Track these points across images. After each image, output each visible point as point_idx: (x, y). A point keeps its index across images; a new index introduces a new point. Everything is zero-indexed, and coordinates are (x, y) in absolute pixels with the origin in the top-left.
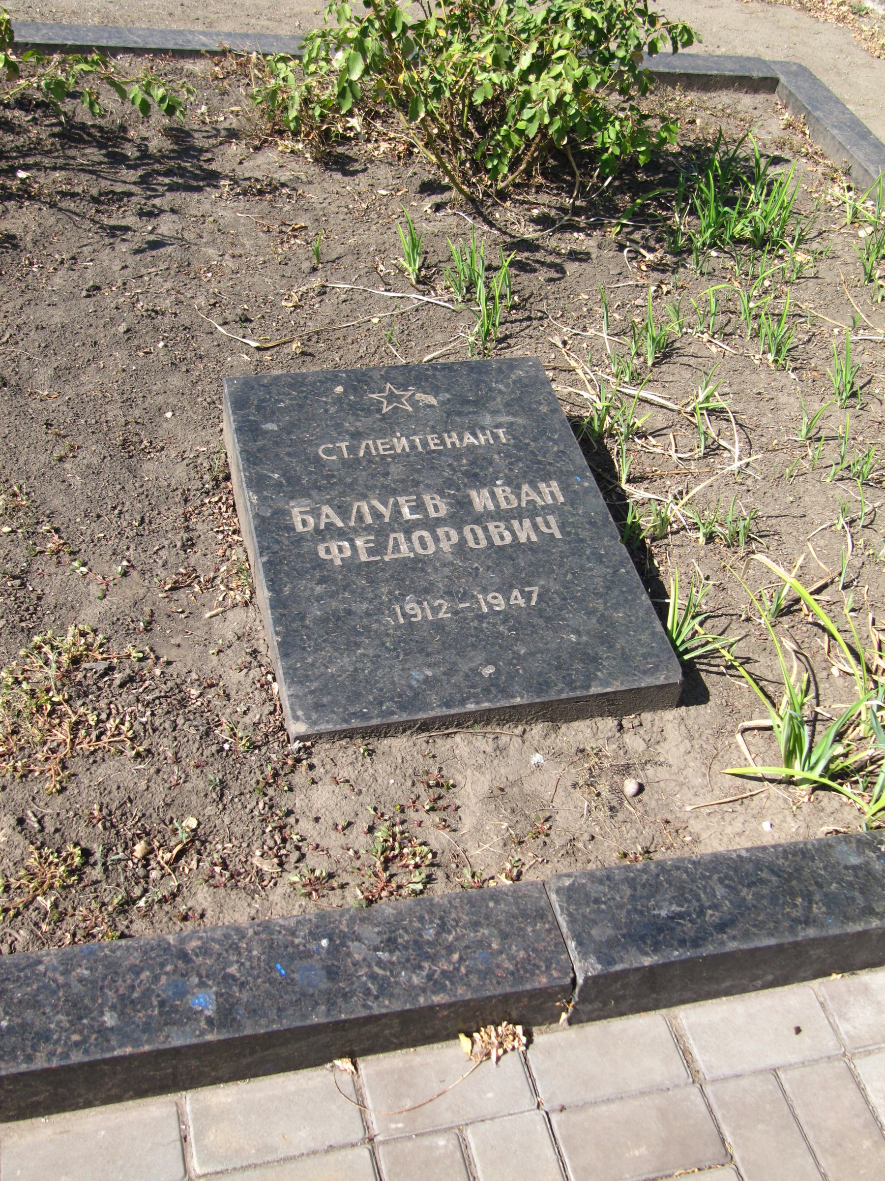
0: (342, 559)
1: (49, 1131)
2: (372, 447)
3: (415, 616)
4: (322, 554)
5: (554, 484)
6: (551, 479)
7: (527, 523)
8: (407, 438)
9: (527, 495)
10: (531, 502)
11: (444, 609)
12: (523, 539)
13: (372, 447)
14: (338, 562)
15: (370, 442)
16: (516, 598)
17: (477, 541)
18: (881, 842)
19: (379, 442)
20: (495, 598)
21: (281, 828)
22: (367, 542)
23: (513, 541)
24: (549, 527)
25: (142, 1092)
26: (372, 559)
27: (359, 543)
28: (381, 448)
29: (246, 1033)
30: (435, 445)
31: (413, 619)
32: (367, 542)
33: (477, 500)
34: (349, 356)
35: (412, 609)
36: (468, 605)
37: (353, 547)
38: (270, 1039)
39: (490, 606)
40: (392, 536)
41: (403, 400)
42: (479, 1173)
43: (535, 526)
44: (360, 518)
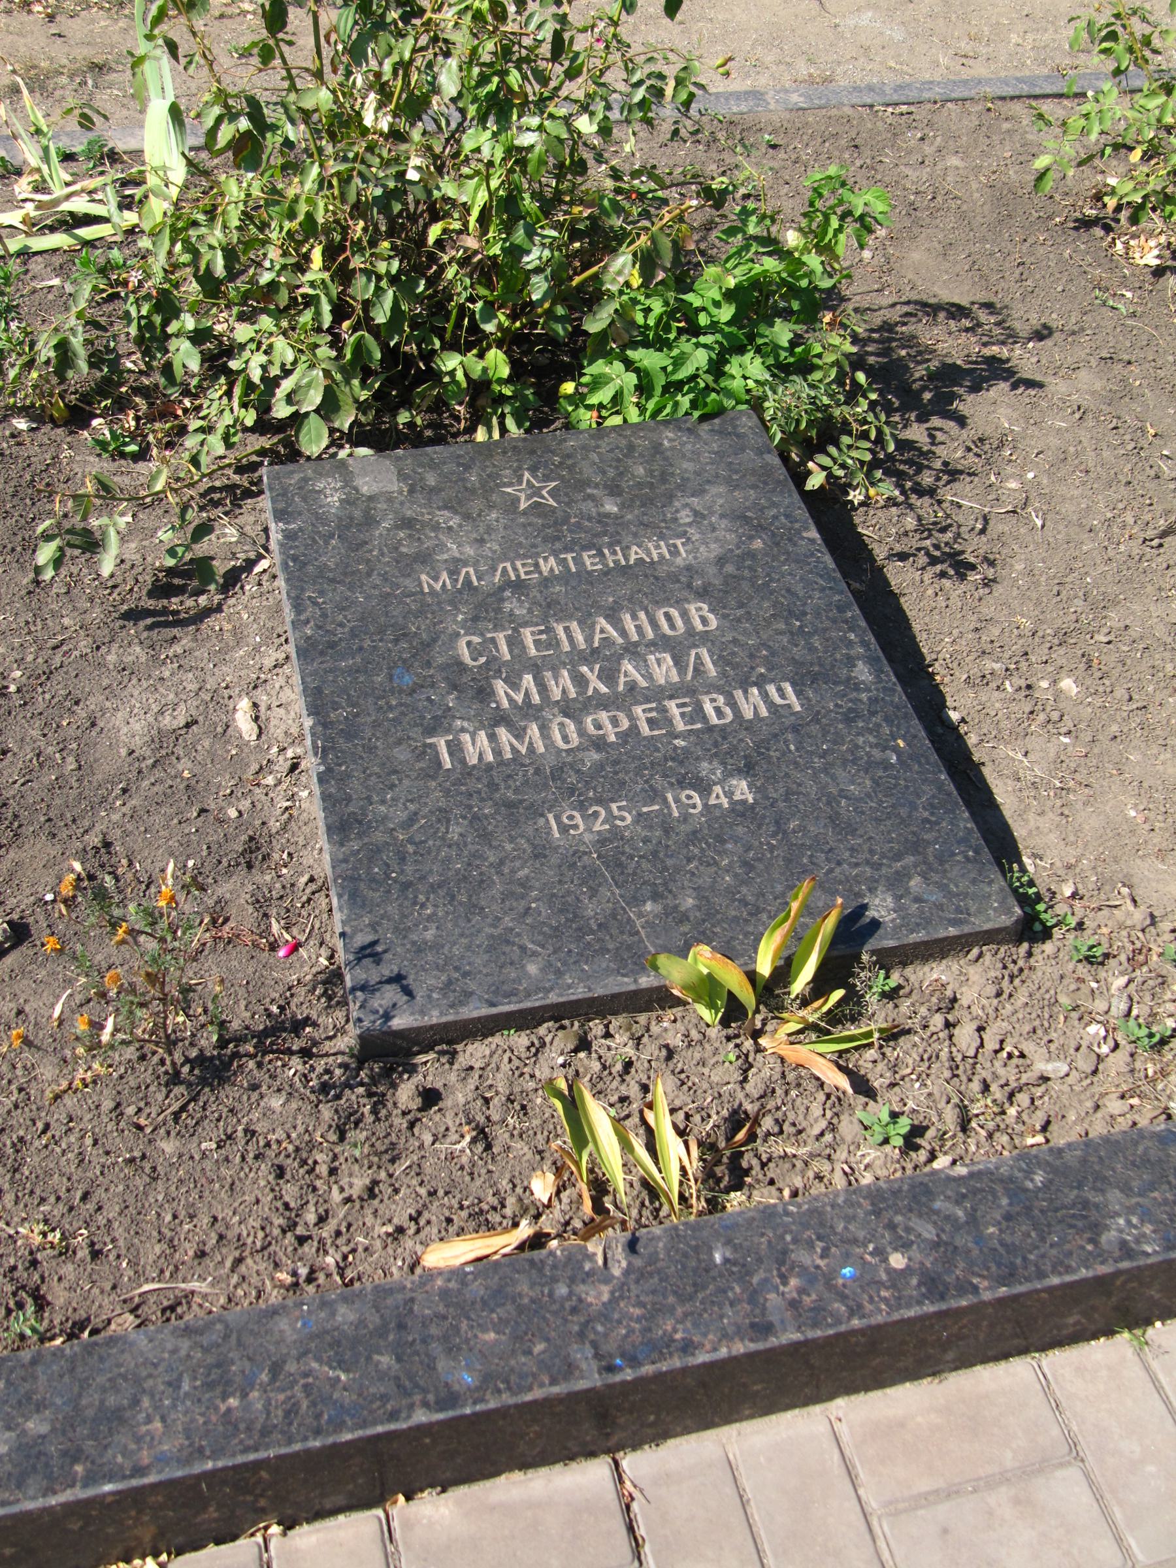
0: (616, 734)
1: (313, 1539)
2: (510, 569)
7: (556, 695)
8: (556, 557)
13: (510, 569)
15: (508, 565)
16: (718, 797)
19: (518, 564)
22: (684, 705)
25: (769, 1406)
26: (656, 733)
27: (638, 710)
28: (522, 571)
29: (582, 1385)
31: (618, 823)
32: (684, 705)
36: (656, 807)
37: (632, 718)
38: (875, 1336)
41: (544, 492)
42: (769, 1560)
43: (765, 696)
44: (699, 670)
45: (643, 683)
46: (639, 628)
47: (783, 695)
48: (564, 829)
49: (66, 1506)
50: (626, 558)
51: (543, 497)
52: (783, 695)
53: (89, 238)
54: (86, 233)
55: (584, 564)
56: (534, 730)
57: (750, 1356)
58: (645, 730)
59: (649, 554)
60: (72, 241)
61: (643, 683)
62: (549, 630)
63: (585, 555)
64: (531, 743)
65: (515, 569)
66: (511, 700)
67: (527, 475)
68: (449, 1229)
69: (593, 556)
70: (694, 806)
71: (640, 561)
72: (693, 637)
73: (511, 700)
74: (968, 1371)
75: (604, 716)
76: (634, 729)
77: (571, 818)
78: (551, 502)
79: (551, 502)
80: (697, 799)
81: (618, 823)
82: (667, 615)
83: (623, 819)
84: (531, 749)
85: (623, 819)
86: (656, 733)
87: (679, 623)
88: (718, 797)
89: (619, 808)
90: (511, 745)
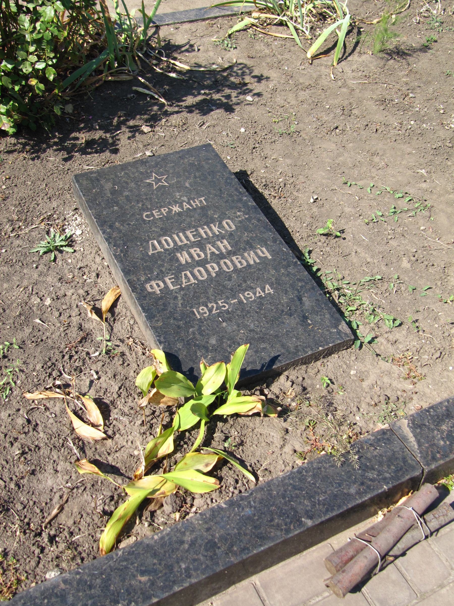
3: (251, 298)
4: (150, 290)
5: (225, 242)
6: (183, 250)
9: (210, 249)
10: (213, 254)
11: (215, 309)
12: (252, 262)
14: (159, 292)
16: (259, 293)
17: (228, 267)
18: (136, 603)
20: (248, 294)
21: (43, 518)
23: (234, 268)
24: (264, 253)
31: (223, 309)
33: (181, 258)
34: (43, 195)
35: (202, 309)
39: (247, 299)
40: (183, 273)
43: (256, 254)
45: (217, 252)
46: (205, 232)
47: (264, 253)
48: (247, 299)
51: (163, 183)
57: (169, 596)
58: (172, 287)
61: (217, 252)
62: (197, 230)
63: (154, 212)
67: (154, 174)
68: (100, 528)
69: (157, 212)
70: (205, 313)
75: (154, 283)
76: (166, 287)
77: (202, 309)
81: (223, 309)
83: (225, 307)
85: (225, 307)
86: (175, 288)
88: (259, 293)
89: (222, 303)
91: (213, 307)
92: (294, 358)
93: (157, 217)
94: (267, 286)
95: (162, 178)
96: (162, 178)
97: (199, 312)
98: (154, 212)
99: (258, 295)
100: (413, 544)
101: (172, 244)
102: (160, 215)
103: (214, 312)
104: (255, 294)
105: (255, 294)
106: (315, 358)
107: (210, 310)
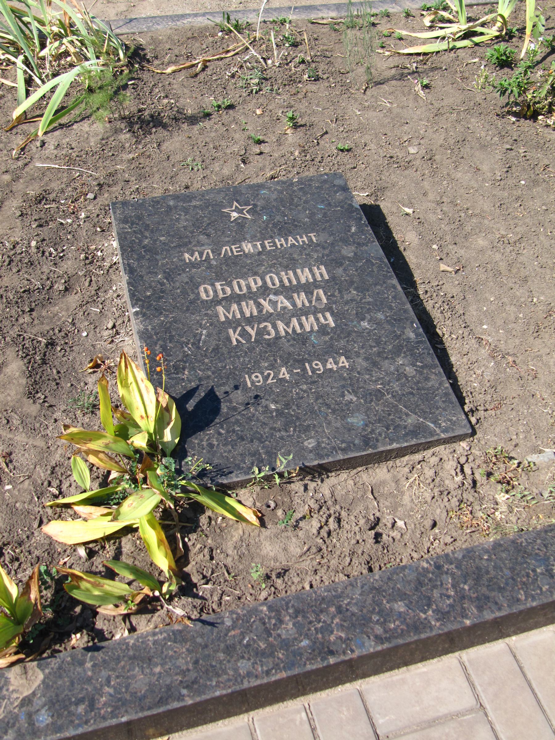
15: (228, 248)
16: (284, 374)
20: (317, 365)
28: (234, 250)
30: (270, 246)
33: (298, 300)
41: (245, 212)
43: (317, 319)
47: (326, 319)
49: (164, 712)
50: (287, 243)
52: (326, 319)
53: (477, 42)
54: (477, 39)
55: (265, 247)
56: (294, 321)
59: (298, 242)
60: (471, 43)
63: (266, 242)
64: (294, 328)
65: (231, 250)
66: (226, 317)
70: (259, 382)
71: (293, 245)
72: (316, 285)
73: (226, 317)
74: (539, 630)
78: (249, 217)
79: (249, 217)
80: (320, 366)
82: (271, 278)
84: (294, 330)
87: (211, 293)
88: (284, 374)
90: (284, 329)
91: (269, 375)
92: (426, 438)
93: (235, 254)
94: (343, 358)
95: (244, 209)
96: (244, 209)
97: (311, 367)
98: (266, 242)
99: (341, 365)
100: (523, 679)
101: (245, 290)
102: (272, 246)
103: (270, 381)
104: (324, 366)
105: (324, 366)
106: (242, 485)
107: (266, 378)
